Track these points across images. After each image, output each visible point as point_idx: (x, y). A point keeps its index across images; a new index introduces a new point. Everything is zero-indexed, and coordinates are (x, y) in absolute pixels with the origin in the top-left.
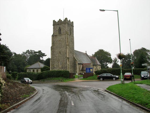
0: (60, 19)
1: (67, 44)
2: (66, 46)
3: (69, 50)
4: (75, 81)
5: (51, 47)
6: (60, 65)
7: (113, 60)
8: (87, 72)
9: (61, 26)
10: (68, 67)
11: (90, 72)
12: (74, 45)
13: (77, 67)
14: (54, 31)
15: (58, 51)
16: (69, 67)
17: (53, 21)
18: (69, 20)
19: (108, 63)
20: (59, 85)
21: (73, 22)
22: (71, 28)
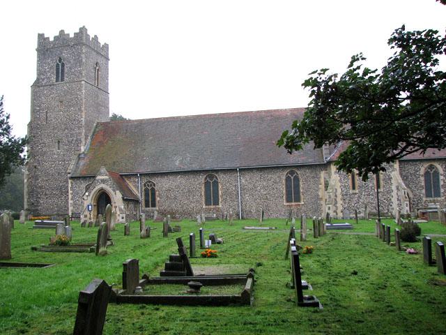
0: (62, 32)
18: (92, 36)
21: (106, 46)
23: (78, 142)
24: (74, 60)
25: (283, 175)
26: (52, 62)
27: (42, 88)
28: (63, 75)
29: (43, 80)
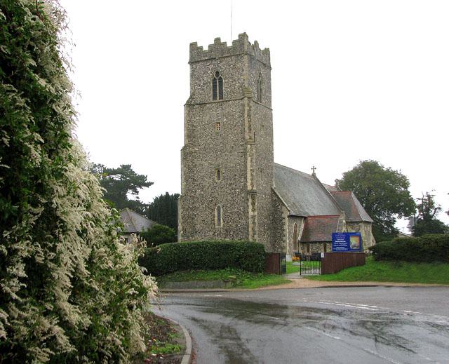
0: (217, 40)
1: (247, 137)
2: (242, 145)
3: (254, 161)
4: (290, 285)
5: (184, 150)
6: (219, 220)
7: (418, 203)
8: (338, 249)
9: (223, 67)
10: (250, 229)
11: (349, 249)
12: (274, 141)
13: (286, 227)
14: (193, 86)
15: (210, 164)
16: (256, 229)
17: (191, 45)
18: (252, 43)
19: (395, 216)
20: (238, 300)
21: (267, 51)
22: (260, 75)
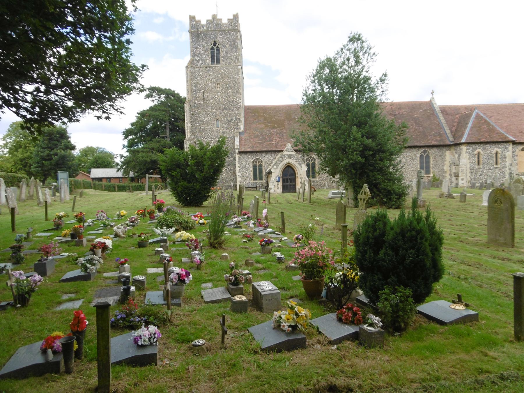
0: (214, 17)
23: (237, 121)
24: (230, 45)
25: (418, 153)
26: (206, 45)
27: (197, 69)
28: (218, 59)
29: (198, 61)
